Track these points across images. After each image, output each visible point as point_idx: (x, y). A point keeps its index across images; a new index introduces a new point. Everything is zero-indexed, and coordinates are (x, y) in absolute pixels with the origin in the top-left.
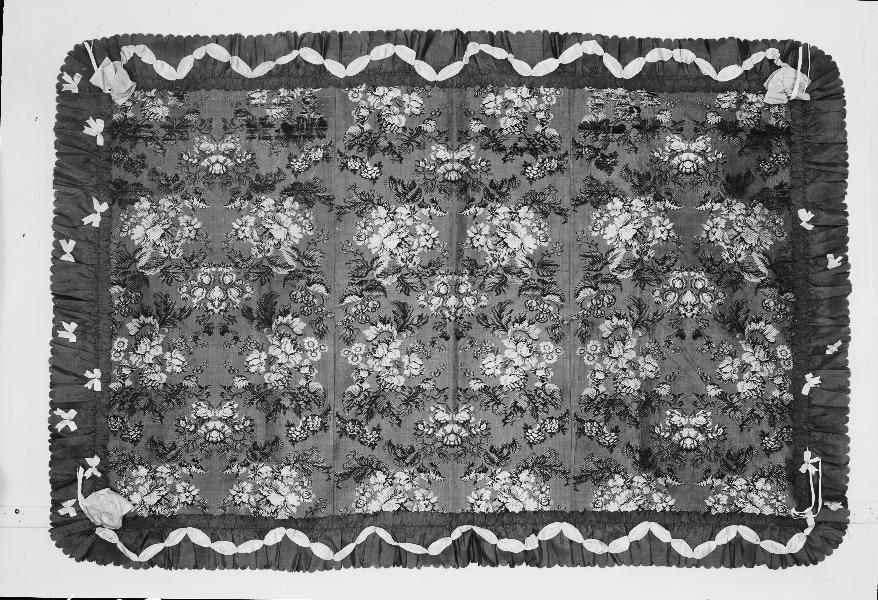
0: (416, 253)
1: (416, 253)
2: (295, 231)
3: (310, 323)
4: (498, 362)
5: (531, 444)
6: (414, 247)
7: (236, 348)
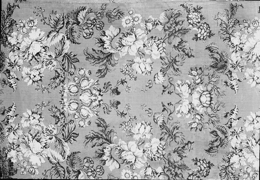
0: (45, 127)
1: (45, 127)
2: (34, 35)
3: (110, 22)
4: (140, 61)
5: (210, 35)
6: (40, 129)
7: (131, 83)
